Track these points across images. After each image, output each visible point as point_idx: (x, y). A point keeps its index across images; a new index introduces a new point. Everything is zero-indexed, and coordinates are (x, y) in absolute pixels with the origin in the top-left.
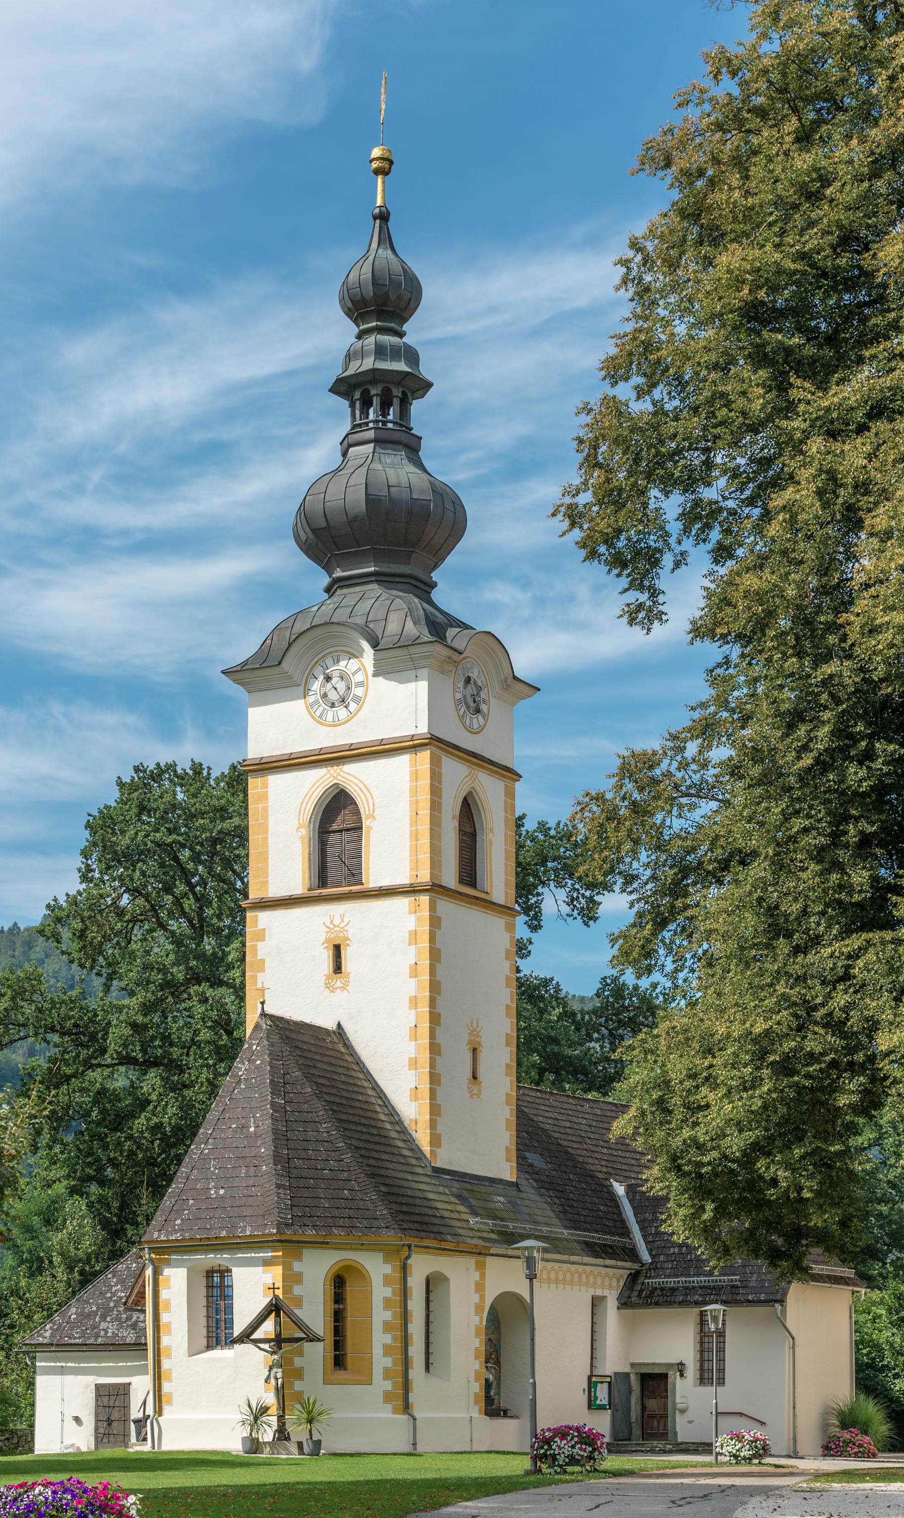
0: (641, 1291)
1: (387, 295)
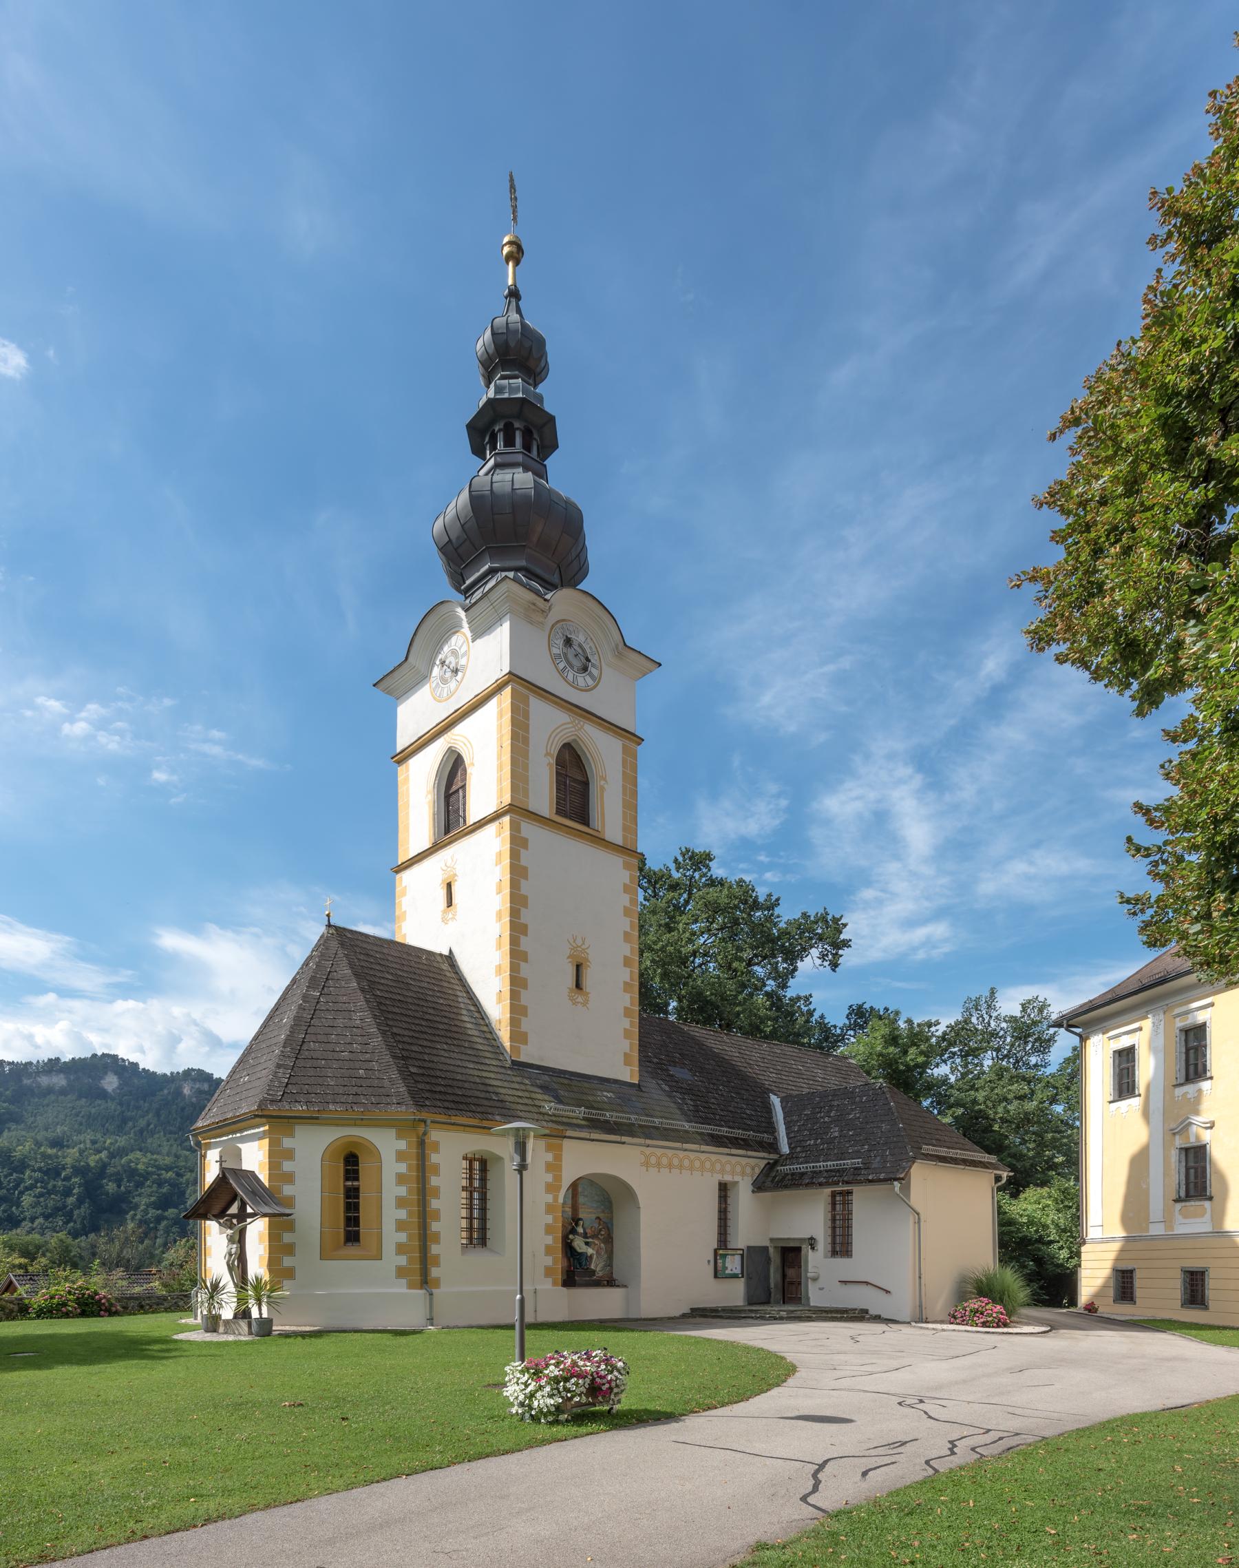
0: (775, 1177)
1: (506, 342)
